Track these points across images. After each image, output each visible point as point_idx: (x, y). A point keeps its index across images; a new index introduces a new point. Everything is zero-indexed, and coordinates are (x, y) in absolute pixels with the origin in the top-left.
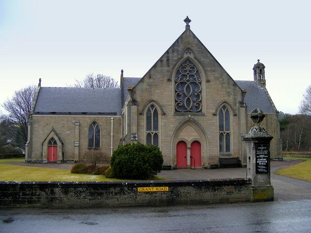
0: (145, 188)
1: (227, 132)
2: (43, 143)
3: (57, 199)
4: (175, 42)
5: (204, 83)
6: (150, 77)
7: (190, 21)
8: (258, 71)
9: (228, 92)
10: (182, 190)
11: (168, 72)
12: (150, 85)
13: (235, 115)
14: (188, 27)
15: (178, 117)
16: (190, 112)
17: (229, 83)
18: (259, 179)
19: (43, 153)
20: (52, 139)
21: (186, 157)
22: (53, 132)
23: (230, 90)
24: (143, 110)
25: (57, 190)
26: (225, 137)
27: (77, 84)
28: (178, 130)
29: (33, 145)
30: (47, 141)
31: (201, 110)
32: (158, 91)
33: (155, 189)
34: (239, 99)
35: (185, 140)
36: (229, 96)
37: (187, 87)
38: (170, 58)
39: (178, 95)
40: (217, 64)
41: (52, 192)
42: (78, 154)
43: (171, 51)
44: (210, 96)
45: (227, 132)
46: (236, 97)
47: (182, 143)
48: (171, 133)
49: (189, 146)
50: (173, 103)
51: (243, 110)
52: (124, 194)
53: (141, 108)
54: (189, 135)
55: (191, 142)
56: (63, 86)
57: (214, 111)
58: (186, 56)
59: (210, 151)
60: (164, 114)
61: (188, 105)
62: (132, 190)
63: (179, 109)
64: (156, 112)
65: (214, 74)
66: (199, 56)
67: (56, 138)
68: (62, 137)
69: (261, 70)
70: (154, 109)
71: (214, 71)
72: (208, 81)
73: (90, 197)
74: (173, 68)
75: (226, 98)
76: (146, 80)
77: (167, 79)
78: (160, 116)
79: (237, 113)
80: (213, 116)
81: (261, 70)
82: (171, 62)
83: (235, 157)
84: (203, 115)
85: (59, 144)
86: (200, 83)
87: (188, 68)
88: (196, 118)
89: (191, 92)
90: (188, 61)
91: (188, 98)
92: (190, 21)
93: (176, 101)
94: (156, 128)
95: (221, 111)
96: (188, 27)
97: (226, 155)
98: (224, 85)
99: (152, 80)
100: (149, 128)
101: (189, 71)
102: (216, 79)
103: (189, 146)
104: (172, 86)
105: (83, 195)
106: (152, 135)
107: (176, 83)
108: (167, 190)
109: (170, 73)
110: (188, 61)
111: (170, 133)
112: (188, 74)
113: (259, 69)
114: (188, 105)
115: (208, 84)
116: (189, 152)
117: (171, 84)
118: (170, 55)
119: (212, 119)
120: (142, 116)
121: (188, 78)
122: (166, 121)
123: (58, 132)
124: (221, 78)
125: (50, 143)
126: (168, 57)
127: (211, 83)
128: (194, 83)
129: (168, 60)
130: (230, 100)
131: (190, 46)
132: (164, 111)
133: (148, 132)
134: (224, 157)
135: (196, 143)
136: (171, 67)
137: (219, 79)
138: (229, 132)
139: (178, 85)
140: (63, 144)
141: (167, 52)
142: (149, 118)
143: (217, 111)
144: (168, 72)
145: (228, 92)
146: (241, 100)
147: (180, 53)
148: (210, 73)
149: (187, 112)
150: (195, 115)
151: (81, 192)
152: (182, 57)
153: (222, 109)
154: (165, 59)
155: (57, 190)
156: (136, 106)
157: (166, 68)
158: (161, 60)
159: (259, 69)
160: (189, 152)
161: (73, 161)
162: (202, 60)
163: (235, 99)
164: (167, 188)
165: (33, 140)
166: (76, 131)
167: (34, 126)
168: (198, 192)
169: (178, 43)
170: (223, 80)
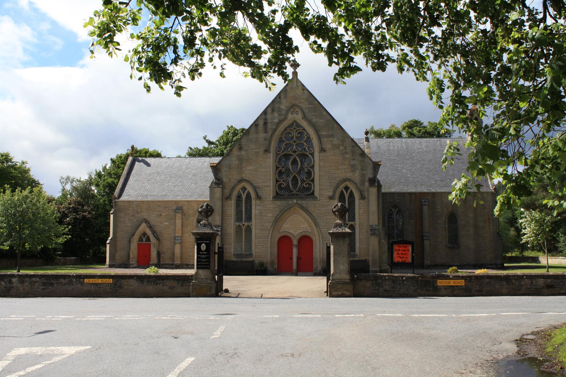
0: (91, 280)
1: (350, 223)
3: (14, 287)
4: (276, 98)
5: (316, 154)
6: (240, 149)
7: (298, 65)
9: (353, 166)
10: (124, 282)
11: (265, 140)
12: (240, 159)
15: (278, 203)
16: (296, 195)
19: (131, 254)
21: (291, 258)
22: (144, 225)
24: (231, 194)
25: (14, 280)
28: (278, 220)
29: (118, 242)
31: (313, 192)
32: (252, 168)
33: (100, 281)
34: (370, 175)
35: (289, 235)
36: (354, 171)
38: (269, 121)
39: (280, 173)
40: (336, 125)
41: (10, 282)
43: (269, 111)
44: (326, 172)
45: (350, 223)
46: (365, 172)
48: (269, 225)
49: (295, 242)
51: (374, 190)
52: (73, 284)
53: (227, 191)
55: (298, 237)
57: (331, 194)
60: (259, 197)
62: (80, 281)
65: (332, 141)
70: (349, 192)
71: (332, 136)
72: (322, 150)
73: (42, 287)
74: (272, 136)
75: (349, 175)
82: (269, 126)
83: (361, 259)
85: (153, 240)
86: (312, 154)
87: (295, 134)
88: (304, 203)
89: (299, 167)
91: (295, 177)
92: (298, 65)
94: (249, 218)
98: (346, 156)
99: (243, 153)
100: (239, 218)
102: (335, 147)
103: (295, 242)
105: (37, 285)
106: (244, 228)
107: (277, 154)
109: (267, 142)
112: (294, 142)
114: (294, 184)
115: (323, 154)
116: (295, 251)
118: (269, 116)
121: (295, 147)
122: (262, 208)
123: (152, 223)
124: (343, 145)
125: (141, 239)
126: (266, 119)
128: (303, 156)
129: (265, 123)
130: (356, 176)
131: (297, 102)
132: (260, 194)
133: (238, 224)
136: (270, 133)
137: (339, 147)
138: (353, 223)
139: (280, 159)
141: (265, 112)
143: (334, 192)
144: (265, 140)
145: (353, 166)
148: (325, 140)
149: (293, 195)
150: (302, 198)
151: (35, 282)
152: (285, 118)
153: (344, 190)
154: (261, 123)
155: (14, 280)
156: (220, 189)
157: (262, 135)
160: (295, 251)
161: (173, 264)
163: (363, 175)
164: (111, 280)
165: (117, 234)
166: (177, 221)
169: (280, 98)
170: (346, 148)
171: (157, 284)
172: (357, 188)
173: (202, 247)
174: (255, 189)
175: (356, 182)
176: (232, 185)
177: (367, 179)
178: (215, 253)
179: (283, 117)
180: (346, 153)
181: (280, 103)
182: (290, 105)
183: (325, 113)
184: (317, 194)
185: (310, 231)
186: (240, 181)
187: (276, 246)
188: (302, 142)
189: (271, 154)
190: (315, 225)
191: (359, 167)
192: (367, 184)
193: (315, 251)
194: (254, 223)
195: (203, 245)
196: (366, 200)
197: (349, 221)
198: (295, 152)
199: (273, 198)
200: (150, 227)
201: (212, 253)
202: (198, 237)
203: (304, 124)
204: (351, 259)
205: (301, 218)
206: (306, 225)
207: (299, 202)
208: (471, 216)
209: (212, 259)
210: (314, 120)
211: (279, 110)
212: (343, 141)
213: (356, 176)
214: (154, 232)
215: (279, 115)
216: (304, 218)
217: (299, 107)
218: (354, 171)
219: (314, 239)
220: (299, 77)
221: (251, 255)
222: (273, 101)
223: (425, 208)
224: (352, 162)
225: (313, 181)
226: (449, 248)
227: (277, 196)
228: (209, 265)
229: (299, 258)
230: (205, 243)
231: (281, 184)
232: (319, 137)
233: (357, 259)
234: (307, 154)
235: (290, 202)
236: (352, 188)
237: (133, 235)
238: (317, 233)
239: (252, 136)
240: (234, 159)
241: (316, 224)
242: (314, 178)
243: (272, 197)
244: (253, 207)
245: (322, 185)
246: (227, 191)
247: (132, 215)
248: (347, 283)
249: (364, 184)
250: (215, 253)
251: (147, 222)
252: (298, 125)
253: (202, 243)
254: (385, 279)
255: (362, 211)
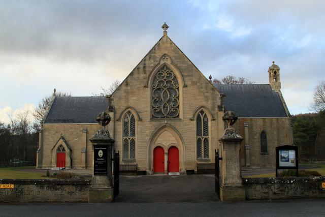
1: (205, 137)
2: (52, 149)
4: (152, 49)
5: (181, 88)
7: (167, 27)
8: (272, 74)
10: (25, 187)
11: (144, 78)
12: (127, 92)
13: (214, 120)
14: (165, 32)
15: (154, 123)
16: (167, 117)
17: (207, 88)
18: (98, 181)
20: (61, 146)
21: (163, 163)
22: (61, 140)
23: (208, 94)
26: (202, 144)
27: (103, 92)
30: (56, 148)
31: (179, 115)
32: (135, 98)
35: (162, 146)
37: (164, 94)
38: (147, 65)
39: (155, 102)
42: (85, 161)
44: (188, 101)
45: (205, 137)
47: (159, 149)
48: (148, 139)
49: (166, 151)
50: (149, 109)
53: (118, 116)
54: (166, 140)
56: (89, 95)
58: (162, 62)
59: (188, 157)
60: (140, 120)
61: (164, 110)
63: (156, 114)
64: (133, 119)
65: (191, 79)
66: (175, 61)
67: (64, 145)
68: (70, 143)
69: (275, 73)
71: (192, 76)
72: (185, 86)
74: (149, 76)
75: (204, 103)
76: (124, 87)
77: (144, 85)
78: (136, 122)
79: (216, 118)
80: (190, 121)
81: (275, 73)
82: (147, 69)
84: (180, 120)
85: (67, 151)
86: (178, 89)
87: (165, 74)
88: (172, 123)
90: (165, 67)
92: (167, 27)
93: (153, 107)
94: (133, 134)
95: (199, 118)
96: (165, 32)
97: (205, 161)
98: (202, 90)
99: (129, 88)
101: (166, 77)
102: (194, 83)
103: (166, 151)
104: (148, 93)
106: (129, 141)
108: (13, 187)
110: (165, 67)
111: (146, 138)
112: (165, 80)
113: (274, 72)
114: (164, 110)
116: (166, 157)
117: (148, 91)
118: (147, 62)
119: (189, 124)
120: (119, 123)
121: (165, 84)
123: (67, 139)
124: (199, 82)
125: (59, 149)
126: (145, 64)
127: (188, 88)
128: (170, 89)
129: (144, 67)
130: (209, 104)
131: (166, 52)
132: (141, 117)
134: (202, 162)
135: (173, 150)
136: (148, 74)
137: (196, 84)
140: (71, 150)
141: (144, 60)
142: (125, 124)
143: (194, 116)
144: (144, 78)
146: (220, 104)
147: (158, 59)
152: (159, 64)
154: (142, 66)
156: (113, 113)
157: (142, 75)
158: (137, 68)
159: (274, 72)
160: (166, 157)
162: (179, 65)
164: (13, 185)
165: (44, 147)
167: (44, 133)
168: (40, 190)
169: (155, 49)
170: (201, 84)
171: (56, 189)
172: (210, 112)
173: (99, 153)
174: (138, 113)
175: (209, 108)
176: (122, 110)
177: (216, 106)
178: (112, 160)
179: (157, 63)
180: (202, 88)
181: (155, 53)
182: (162, 54)
183: (186, 60)
184: (181, 116)
185: (176, 143)
186: (128, 108)
187: (152, 154)
188: (171, 80)
189: (149, 88)
190: (180, 138)
191: (211, 98)
192: (217, 109)
193: (180, 160)
194: (136, 138)
195: (101, 151)
196: (216, 121)
197: (204, 135)
198: (165, 87)
199: (150, 119)
200: (66, 142)
201: (109, 161)
202: (96, 144)
203: (172, 67)
204: (198, 162)
205: (170, 134)
206: (173, 139)
207: (169, 122)
208: (275, 133)
209: (109, 165)
210: (179, 65)
211: (155, 58)
212: (199, 79)
213: (209, 104)
214: (68, 145)
215: (154, 61)
216: (172, 134)
217: (168, 55)
218: (207, 100)
219: (179, 148)
220: (168, 35)
221: (135, 161)
222: (150, 52)
223: (246, 129)
224: (206, 94)
225: (178, 107)
226: (262, 154)
227: (153, 118)
228: (106, 171)
229: (168, 162)
230: (102, 150)
231: (156, 109)
232: (183, 77)
233: (210, 162)
234: (174, 88)
235: (163, 122)
236: (206, 112)
237: (54, 147)
238: (181, 144)
239: (135, 76)
240: (123, 92)
241: (181, 139)
242: (179, 105)
243: (149, 118)
244: (136, 126)
245: (186, 109)
246: (118, 116)
247: (54, 134)
248: (240, 187)
249: (214, 110)
250: (112, 160)
251: (63, 138)
252: (168, 68)
253: (99, 150)
254: (274, 183)
255: (213, 128)
